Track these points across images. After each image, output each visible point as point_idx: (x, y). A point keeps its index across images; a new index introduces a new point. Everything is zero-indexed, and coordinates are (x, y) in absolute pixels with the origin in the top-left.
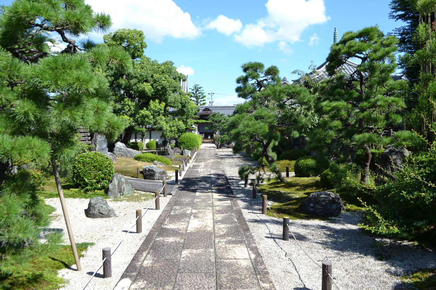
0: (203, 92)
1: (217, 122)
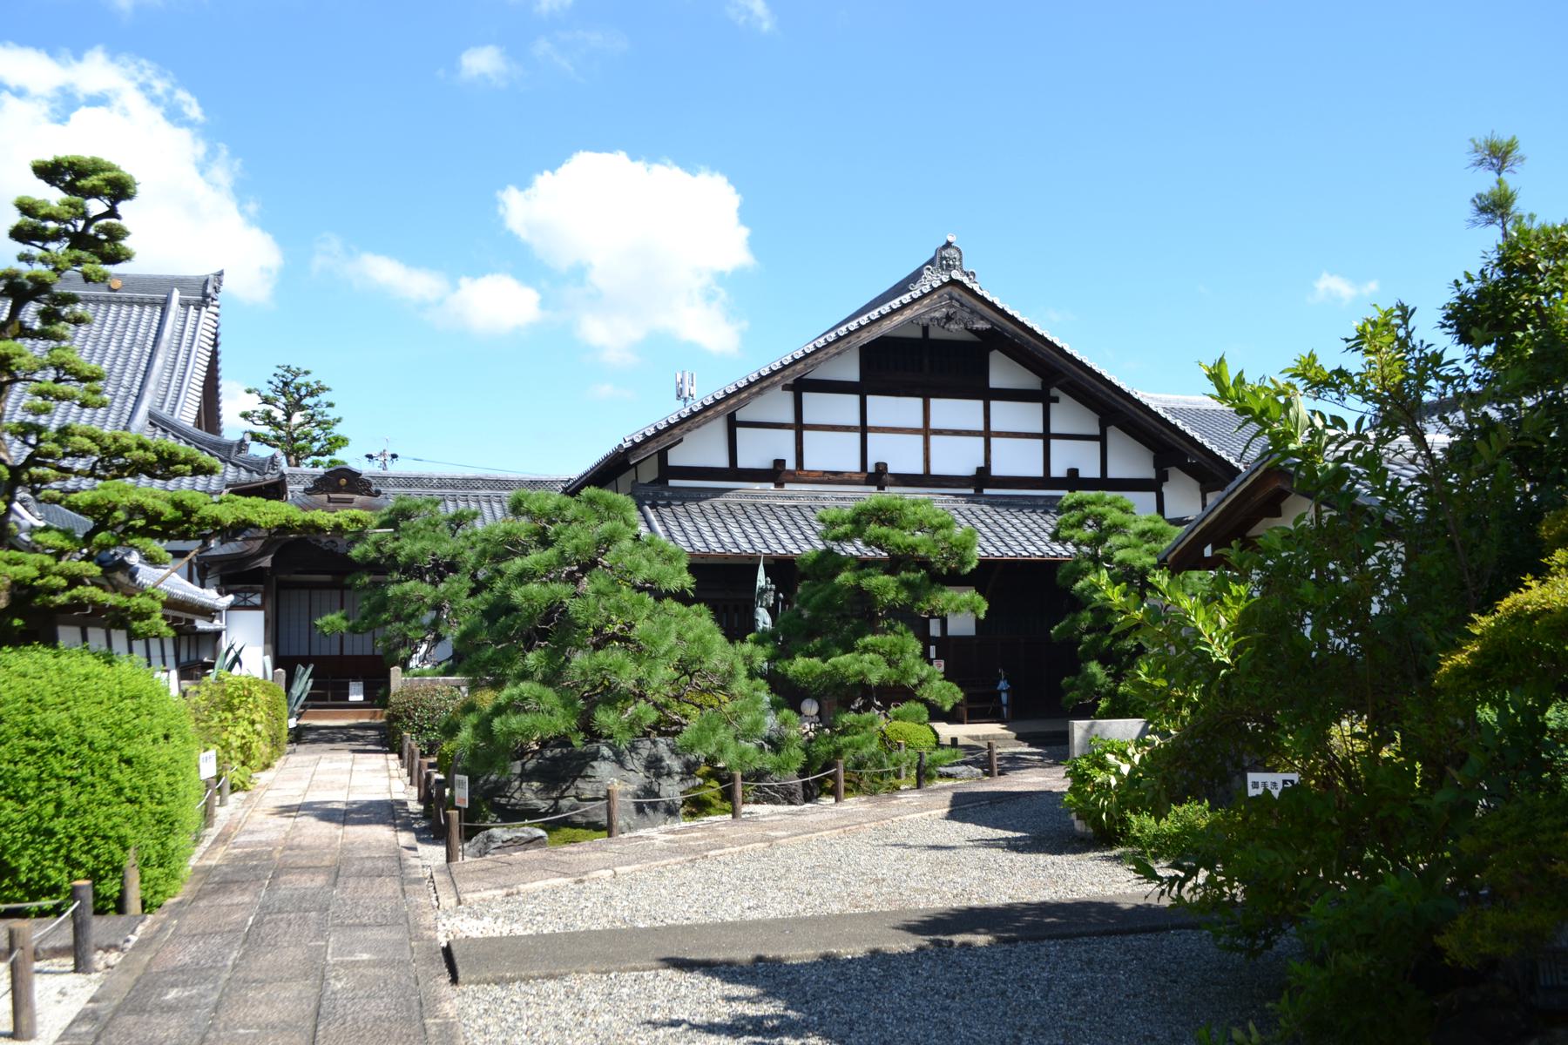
0: (332, 414)
1: (420, 575)
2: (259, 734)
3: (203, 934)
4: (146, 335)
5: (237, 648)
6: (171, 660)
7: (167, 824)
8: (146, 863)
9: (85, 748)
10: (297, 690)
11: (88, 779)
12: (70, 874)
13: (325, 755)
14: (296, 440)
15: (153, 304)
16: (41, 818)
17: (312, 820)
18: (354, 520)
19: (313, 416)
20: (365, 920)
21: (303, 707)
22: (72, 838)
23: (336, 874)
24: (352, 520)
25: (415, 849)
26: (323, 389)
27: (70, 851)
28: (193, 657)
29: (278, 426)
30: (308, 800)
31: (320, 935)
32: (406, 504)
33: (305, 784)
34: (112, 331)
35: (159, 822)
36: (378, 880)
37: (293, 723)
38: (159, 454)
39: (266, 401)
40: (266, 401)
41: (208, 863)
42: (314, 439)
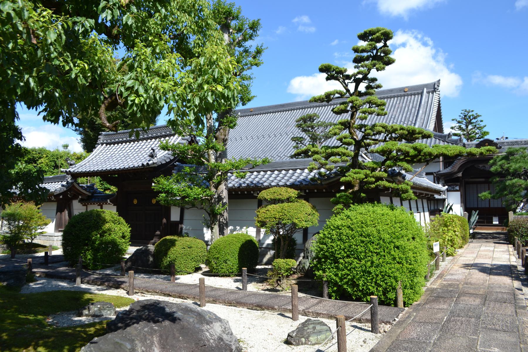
0: (482, 124)
1: (519, 176)
2: (457, 236)
3: (425, 323)
4: (417, 104)
5: (451, 205)
6: (426, 209)
7: (413, 273)
8: (405, 287)
9: (381, 242)
10: (472, 220)
11: (383, 253)
12: (377, 288)
13: (483, 244)
14: (470, 134)
15: (418, 94)
16: (366, 267)
17: (477, 271)
18: (489, 150)
19: (475, 126)
20: (497, 327)
21: (475, 225)
22: (377, 275)
23: (485, 298)
24: (488, 151)
25: (521, 290)
26: (479, 116)
27: (376, 280)
28: (436, 208)
29: (464, 130)
30: (476, 262)
31: (475, 333)
32: (512, 150)
33: (475, 255)
34: (406, 104)
35: (410, 272)
36: (504, 304)
37: (471, 231)
38: (408, 131)
39: (459, 122)
40: (459, 122)
41: (433, 287)
42: (476, 134)
